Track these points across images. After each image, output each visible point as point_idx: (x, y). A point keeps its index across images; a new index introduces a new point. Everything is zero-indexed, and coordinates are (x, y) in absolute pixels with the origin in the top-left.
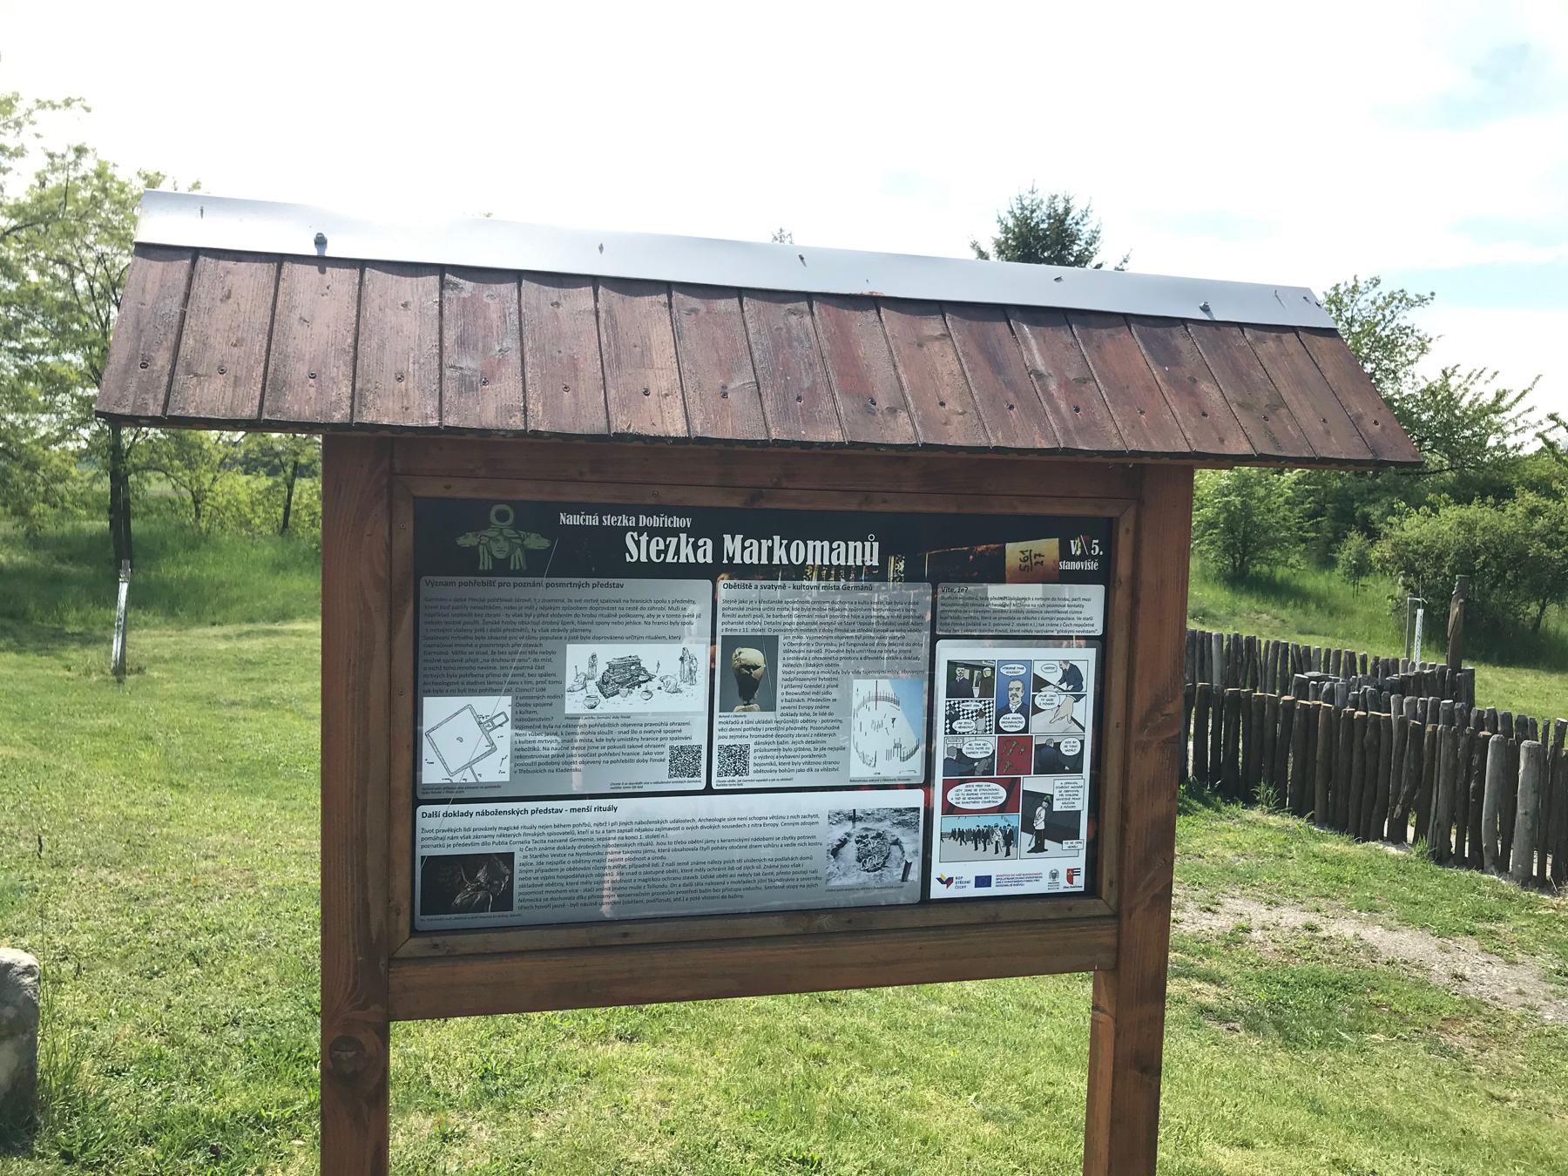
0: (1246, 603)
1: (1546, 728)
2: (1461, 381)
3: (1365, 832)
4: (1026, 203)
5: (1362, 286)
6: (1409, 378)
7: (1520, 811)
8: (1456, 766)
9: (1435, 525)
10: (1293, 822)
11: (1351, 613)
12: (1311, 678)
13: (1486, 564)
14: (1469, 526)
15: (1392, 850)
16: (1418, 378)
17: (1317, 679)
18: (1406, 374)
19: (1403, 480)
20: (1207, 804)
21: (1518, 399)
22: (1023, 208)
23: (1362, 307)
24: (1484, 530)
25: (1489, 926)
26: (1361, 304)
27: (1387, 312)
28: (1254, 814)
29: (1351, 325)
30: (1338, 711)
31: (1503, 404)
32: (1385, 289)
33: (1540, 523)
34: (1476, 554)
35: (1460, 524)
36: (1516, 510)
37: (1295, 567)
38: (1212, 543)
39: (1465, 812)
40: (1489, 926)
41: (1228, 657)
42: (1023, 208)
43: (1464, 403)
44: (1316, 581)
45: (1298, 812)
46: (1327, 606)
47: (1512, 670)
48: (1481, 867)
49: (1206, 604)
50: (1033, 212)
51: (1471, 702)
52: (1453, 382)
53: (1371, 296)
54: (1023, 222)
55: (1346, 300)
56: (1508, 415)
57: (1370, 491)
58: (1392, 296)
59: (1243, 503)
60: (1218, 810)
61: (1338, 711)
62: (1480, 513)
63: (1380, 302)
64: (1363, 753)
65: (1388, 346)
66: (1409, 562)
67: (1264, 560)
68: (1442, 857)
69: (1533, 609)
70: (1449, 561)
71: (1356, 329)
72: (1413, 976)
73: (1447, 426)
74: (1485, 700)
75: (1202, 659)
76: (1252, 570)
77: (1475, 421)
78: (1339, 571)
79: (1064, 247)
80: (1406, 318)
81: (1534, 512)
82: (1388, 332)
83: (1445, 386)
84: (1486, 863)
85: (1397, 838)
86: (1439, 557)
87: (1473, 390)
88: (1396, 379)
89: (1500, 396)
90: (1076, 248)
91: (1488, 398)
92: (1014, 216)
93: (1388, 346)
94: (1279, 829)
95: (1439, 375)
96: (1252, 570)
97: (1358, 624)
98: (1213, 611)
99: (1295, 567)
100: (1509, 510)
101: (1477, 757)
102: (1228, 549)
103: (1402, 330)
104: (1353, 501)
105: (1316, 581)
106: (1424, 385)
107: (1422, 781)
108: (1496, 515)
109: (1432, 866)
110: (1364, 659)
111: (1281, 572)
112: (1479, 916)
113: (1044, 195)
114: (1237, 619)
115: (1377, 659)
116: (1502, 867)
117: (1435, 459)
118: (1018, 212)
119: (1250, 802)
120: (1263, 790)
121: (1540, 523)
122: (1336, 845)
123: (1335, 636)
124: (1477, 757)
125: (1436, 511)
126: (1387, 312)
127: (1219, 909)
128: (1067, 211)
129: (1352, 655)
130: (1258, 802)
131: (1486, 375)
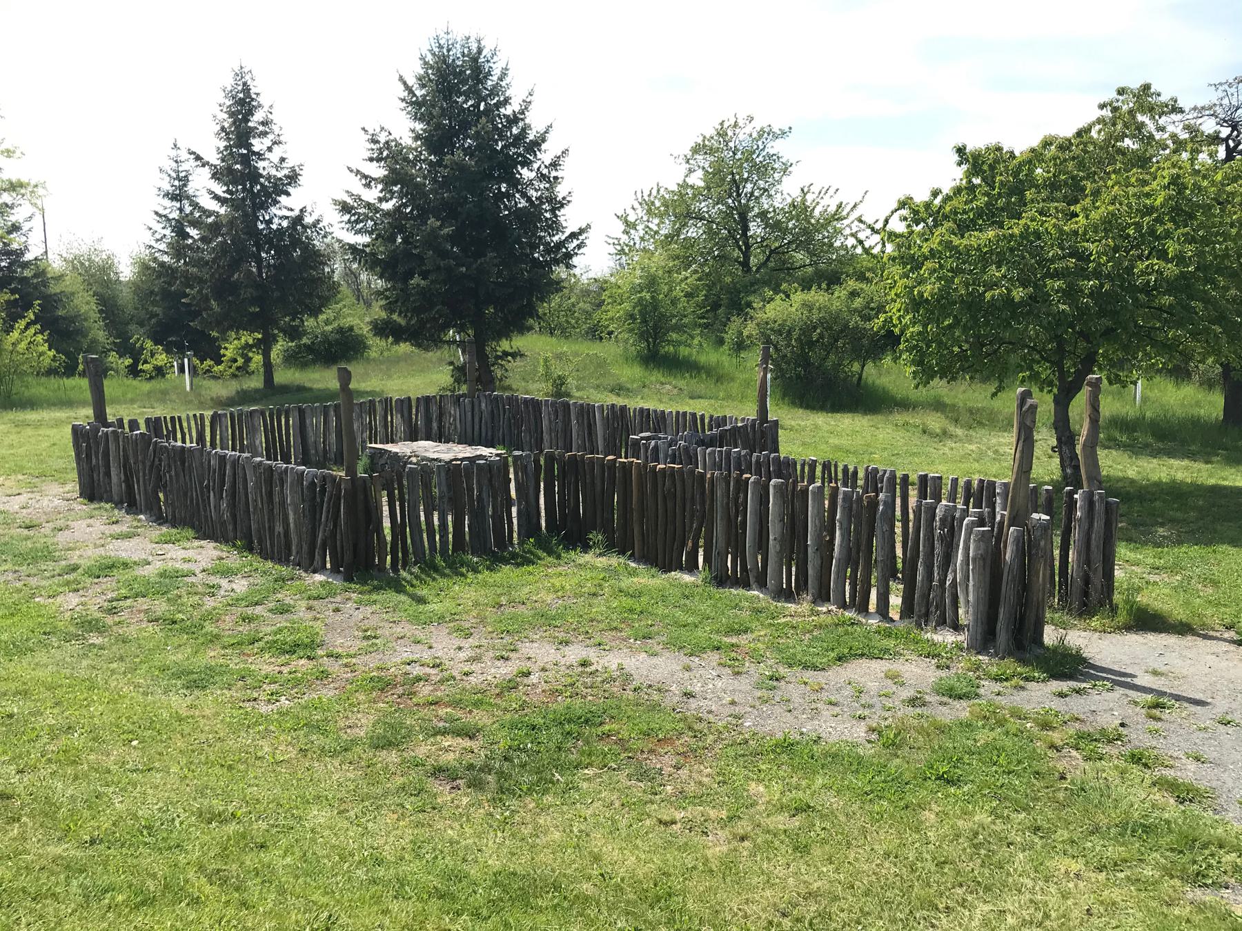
0: (656, 376)
1: (803, 466)
2: (814, 196)
3: (667, 566)
4: (442, 42)
5: (741, 123)
6: (779, 195)
7: (771, 537)
8: (728, 504)
9: (782, 308)
10: (614, 561)
11: (732, 379)
12: (642, 438)
13: (821, 336)
14: (808, 306)
15: (687, 578)
16: (785, 195)
17: (647, 439)
18: (776, 192)
19: (778, 273)
20: (550, 553)
21: (852, 210)
22: (440, 47)
23: (742, 138)
24: (820, 309)
25: (734, 640)
26: (741, 137)
27: (760, 143)
28: (588, 558)
29: (735, 154)
30: (645, 466)
31: (844, 213)
32: (758, 124)
33: (858, 302)
34: (815, 328)
35: (804, 305)
36: (841, 293)
37: (698, 348)
38: (631, 331)
39: (735, 541)
40: (734, 640)
41: (607, 421)
42: (440, 47)
43: (817, 213)
44: (710, 356)
45: (622, 552)
46: (716, 375)
47: (838, 416)
48: (747, 585)
49: (623, 379)
50: (449, 51)
51: (776, 450)
52: (809, 197)
53: (748, 130)
54: (443, 59)
55: (730, 133)
56: (846, 222)
57: (752, 284)
58: (762, 129)
59: (652, 297)
60: (559, 557)
61: (645, 466)
62: (817, 296)
63: (755, 135)
64: (665, 498)
65: (762, 170)
66: (771, 337)
67: (669, 342)
68: (721, 580)
69: (856, 367)
70: (795, 335)
71: (739, 156)
72: (647, 699)
73: (805, 231)
74: (788, 447)
75: (590, 425)
76: (662, 351)
77: (824, 226)
78: (725, 347)
79: (479, 81)
80: (774, 147)
81: (854, 294)
82: (761, 158)
83: (804, 201)
84: (752, 580)
85: (692, 567)
86: (789, 332)
87: (823, 203)
88: (770, 196)
89: (840, 206)
90: (490, 83)
91: (832, 209)
92: (434, 54)
93: (762, 170)
94: (604, 570)
95: (799, 192)
96: (662, 351)
97: (734, 388)
98: (629, 386)
99: (698, 348)
100: (836, 294)
101: (742, 495)
102: (643, 336)
103: (770, 156)
104: (740, 292)
105: (710, 356)
106: (789, 200)
107: (706, 519)
108: (827, 297)
109: (713, 590)
110: (703, 417)
111: (684, 351)
112: (731, 631)
113: (458, 34)
114: (646, 390)
115: (711, 417)
116: (762, 585)
117: (800, 256)
118: (436, 50)
119: (586, 548)
120: (596, 536)
121: (858, 302)
122: (646, 579)
123: (717, 398)
124: (742, 495)
125: (788, 296)
126: (760, 143)
127: (512, 655)
128: (480, 51)
129: (694, 415)
130: (591, 548)
131: (831, 192)
